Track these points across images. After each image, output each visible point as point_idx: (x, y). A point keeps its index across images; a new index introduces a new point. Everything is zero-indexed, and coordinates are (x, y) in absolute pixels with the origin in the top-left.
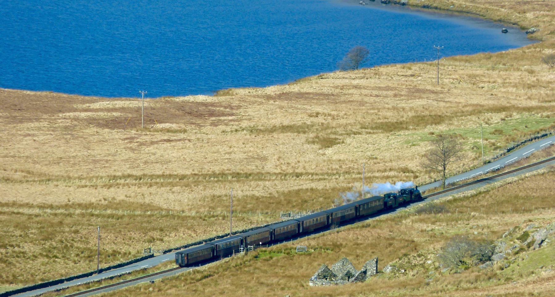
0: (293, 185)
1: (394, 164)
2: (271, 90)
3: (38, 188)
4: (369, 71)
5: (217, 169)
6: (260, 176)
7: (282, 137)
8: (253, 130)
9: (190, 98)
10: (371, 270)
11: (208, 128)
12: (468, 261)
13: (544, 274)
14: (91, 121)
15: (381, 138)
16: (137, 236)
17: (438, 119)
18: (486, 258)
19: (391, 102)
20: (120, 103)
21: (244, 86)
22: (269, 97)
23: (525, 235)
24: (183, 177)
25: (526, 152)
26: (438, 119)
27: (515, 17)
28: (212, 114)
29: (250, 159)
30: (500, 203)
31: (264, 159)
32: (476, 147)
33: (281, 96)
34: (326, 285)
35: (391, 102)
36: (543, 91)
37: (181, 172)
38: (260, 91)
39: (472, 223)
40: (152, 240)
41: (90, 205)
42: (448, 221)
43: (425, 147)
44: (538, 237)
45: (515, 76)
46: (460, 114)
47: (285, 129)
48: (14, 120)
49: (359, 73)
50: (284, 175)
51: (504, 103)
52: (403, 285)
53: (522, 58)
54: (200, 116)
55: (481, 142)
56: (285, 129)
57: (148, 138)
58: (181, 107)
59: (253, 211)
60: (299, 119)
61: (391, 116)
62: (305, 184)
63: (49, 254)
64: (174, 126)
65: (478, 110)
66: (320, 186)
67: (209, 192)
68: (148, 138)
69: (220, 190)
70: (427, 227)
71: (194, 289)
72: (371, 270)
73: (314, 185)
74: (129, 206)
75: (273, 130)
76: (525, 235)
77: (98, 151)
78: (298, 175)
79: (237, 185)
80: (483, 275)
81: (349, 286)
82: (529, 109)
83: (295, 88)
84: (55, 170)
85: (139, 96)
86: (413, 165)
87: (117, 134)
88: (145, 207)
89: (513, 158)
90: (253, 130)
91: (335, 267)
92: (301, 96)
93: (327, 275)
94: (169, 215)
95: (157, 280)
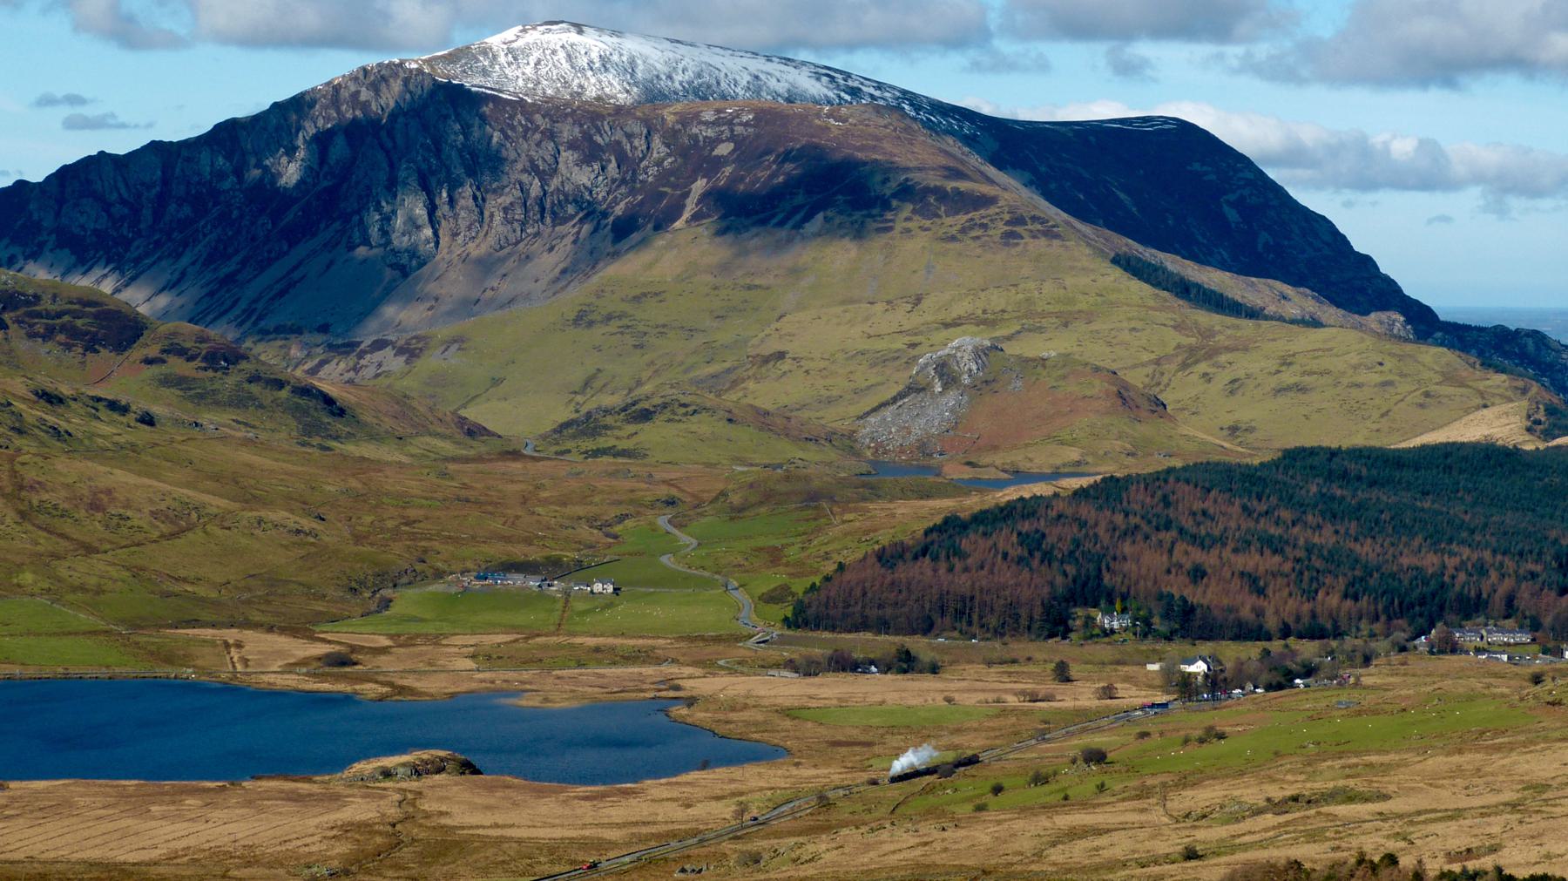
0: (670, 827)
1: (719, 816)
2: (663, 781)
3: (548, 830)
4: (710, 771)
5: (634, 820)
6: (655, 823)
7: (666, 804)
8: (652, 800)
9: (623, 785)
10: (705, 868)
11: (631, 800)
12: (749, 863)
13: (784, 869)
14: (575, 797)
15: (714, 803)
16: (594, 852)
17: (741, 794)
18: (757, 862)
19: (720, 786)
20: (589, 788)
21: (651, 779)
22: (661, 784)
23: (776, 850)
24: (617, 824)
25: (784, 808)
26: (741, 794)
27: (782, 744)
28: (634, 793)
29: (650, 815)
30: (768, 834)
31: (657, 814)
32: (758, 807)
33: (667, 784)
34: (682, 875)
35: (720, 786)
36: (792, 780)
37: (617, 821)
38: (658, 781)
39: (755, 844)
40: (601, 855)
41: (573, 838)
42: (743, 843)
43: (734, 808)
44: (782, 851)
45: (780, 772)
46: (752, 791)
47: (668, 800)
48: (540, 797)
49: (705, 772)
50: (666, 822)
51: (773, 785)
52: (718, 875)
53: (782, 764)
54: (628, 794)
55: (761, 805)
56: (668, 800)
57: (602, 805)
58: (619, 790)
59: (650, 840)
60: (675, 794)
61: (719, 793)
62: (677, 827)
63: (552, 862)
64: (615, 799)
65: (761, 789)
66: (683, 827)
67: (630, 831)
68: (602, 805)
69: (635, 830)
70: (733, 846)
71: (1274, 468)
72: (705, 868)
73: (681, 827)
74: (592, 838)
75: (663, 800)
76: (776, 850)
77: (579, 812)
78: (673, 822)
79: (644, 828)
80: (1523, 586)
81: (693, 876)
82: (785, 788)
83: (674, 780)
84: (557, 821)
85: (597, 784)
86: (728, 817)
87: (588, 804)
88: (599, 839)
89: (776, 812)
90: (652, 800)
91: (687, 867)
92: (677, 783)
93: (683, 871)
94: (610, 842)
95: (602, 874)
